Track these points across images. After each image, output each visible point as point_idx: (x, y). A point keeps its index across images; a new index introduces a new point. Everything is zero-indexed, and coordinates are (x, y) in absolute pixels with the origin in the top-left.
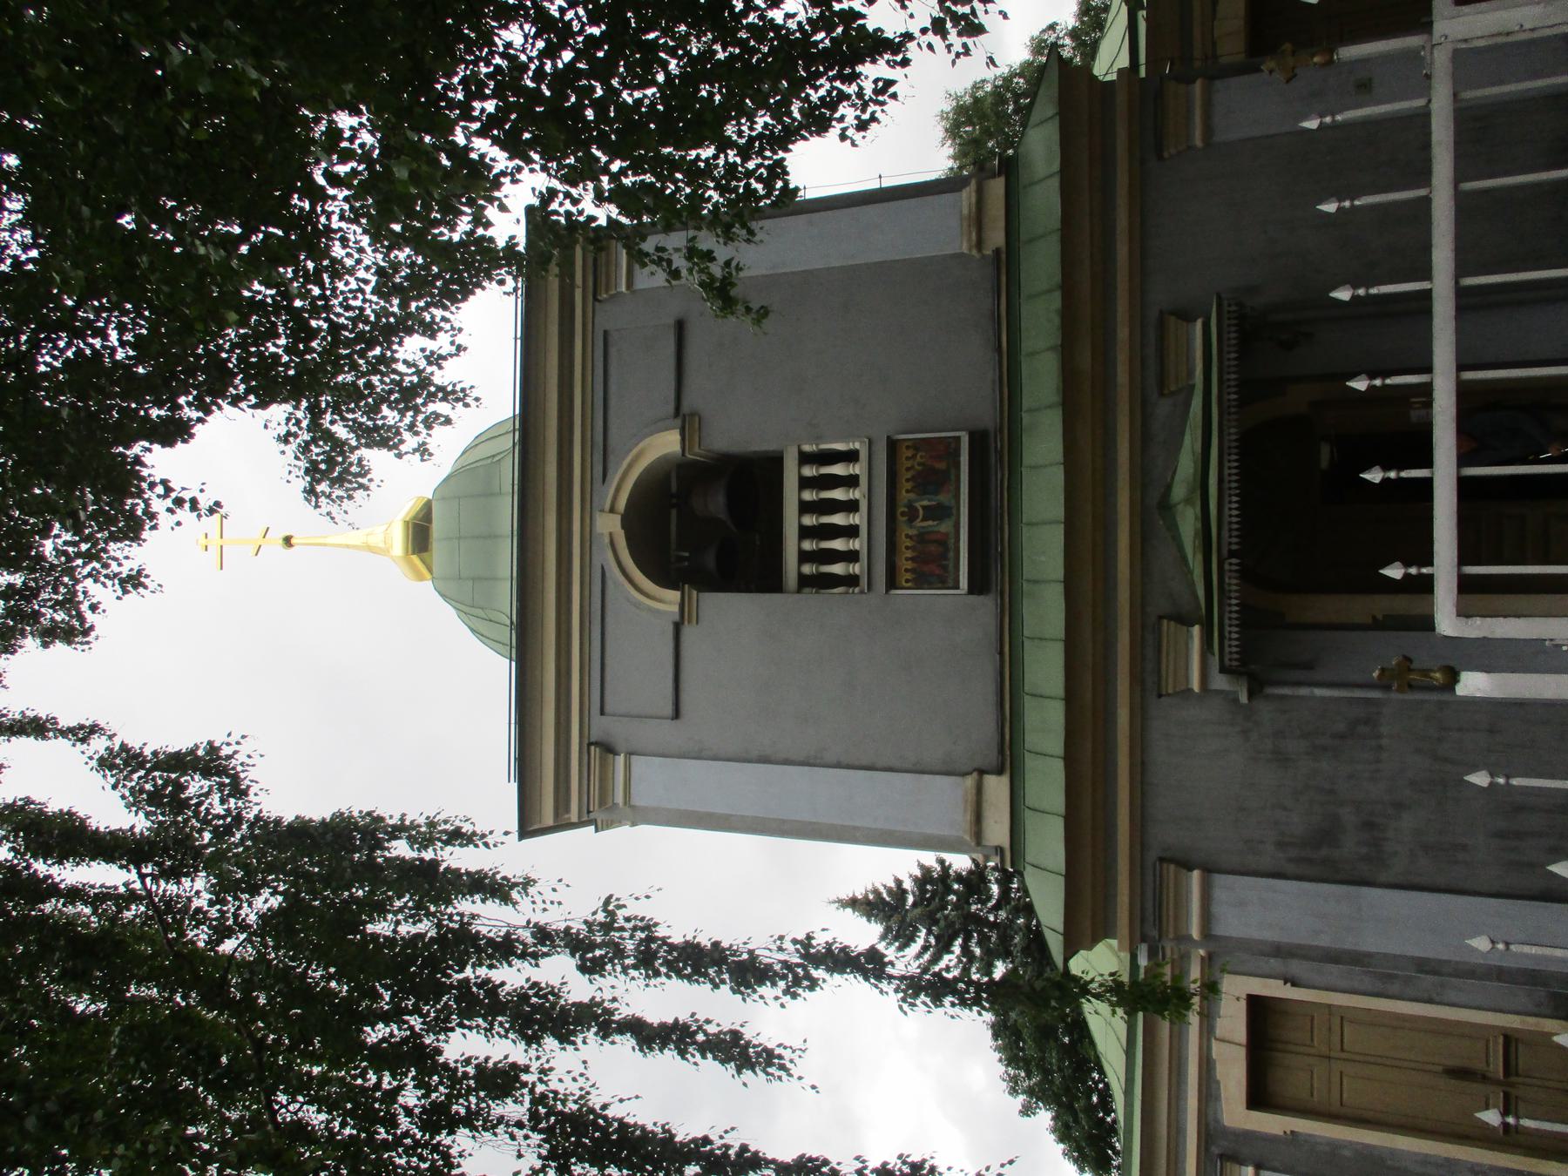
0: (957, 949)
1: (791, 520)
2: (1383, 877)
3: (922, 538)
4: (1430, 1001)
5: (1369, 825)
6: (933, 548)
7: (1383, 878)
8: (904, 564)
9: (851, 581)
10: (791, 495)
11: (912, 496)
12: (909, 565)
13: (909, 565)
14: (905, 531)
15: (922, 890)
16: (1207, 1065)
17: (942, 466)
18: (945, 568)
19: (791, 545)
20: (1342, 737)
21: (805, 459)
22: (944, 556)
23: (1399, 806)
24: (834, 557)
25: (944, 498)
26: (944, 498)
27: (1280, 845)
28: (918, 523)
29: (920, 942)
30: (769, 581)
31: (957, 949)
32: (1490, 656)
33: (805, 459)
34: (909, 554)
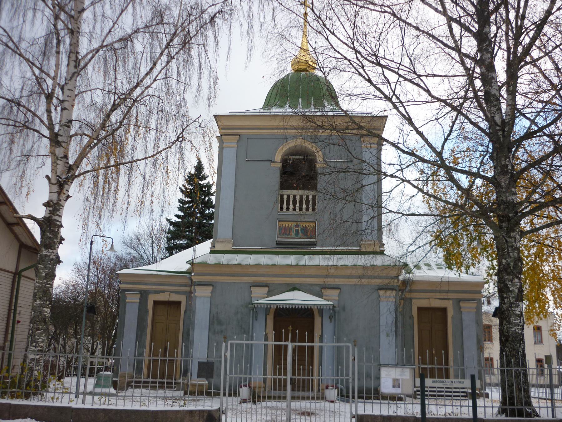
0: (187, 199)
1: (298, 193)
3: (291, 229)
5: (222, 332)
6: (288, 232)
7: (210, 334)
8: (285, 224)
9: (282, 209)
10: (305, 193)
12: (284, 226)
13: (284, 226)
14: (293, 224)
15: (205, 187)
16: (163, 292)
17: (309, 234)
18: (283, 235)
19: (292, 193)
20: (241, 326)
22: (286, 234)
25: (300, 235)
26: (300, 235)
27: (217, 313)
28: (295, 228)
29: (188, 186)
30: (284, 185)
31: (187, 199)
32: (226, 346)
33: (314, 197)
34: (287, 226)
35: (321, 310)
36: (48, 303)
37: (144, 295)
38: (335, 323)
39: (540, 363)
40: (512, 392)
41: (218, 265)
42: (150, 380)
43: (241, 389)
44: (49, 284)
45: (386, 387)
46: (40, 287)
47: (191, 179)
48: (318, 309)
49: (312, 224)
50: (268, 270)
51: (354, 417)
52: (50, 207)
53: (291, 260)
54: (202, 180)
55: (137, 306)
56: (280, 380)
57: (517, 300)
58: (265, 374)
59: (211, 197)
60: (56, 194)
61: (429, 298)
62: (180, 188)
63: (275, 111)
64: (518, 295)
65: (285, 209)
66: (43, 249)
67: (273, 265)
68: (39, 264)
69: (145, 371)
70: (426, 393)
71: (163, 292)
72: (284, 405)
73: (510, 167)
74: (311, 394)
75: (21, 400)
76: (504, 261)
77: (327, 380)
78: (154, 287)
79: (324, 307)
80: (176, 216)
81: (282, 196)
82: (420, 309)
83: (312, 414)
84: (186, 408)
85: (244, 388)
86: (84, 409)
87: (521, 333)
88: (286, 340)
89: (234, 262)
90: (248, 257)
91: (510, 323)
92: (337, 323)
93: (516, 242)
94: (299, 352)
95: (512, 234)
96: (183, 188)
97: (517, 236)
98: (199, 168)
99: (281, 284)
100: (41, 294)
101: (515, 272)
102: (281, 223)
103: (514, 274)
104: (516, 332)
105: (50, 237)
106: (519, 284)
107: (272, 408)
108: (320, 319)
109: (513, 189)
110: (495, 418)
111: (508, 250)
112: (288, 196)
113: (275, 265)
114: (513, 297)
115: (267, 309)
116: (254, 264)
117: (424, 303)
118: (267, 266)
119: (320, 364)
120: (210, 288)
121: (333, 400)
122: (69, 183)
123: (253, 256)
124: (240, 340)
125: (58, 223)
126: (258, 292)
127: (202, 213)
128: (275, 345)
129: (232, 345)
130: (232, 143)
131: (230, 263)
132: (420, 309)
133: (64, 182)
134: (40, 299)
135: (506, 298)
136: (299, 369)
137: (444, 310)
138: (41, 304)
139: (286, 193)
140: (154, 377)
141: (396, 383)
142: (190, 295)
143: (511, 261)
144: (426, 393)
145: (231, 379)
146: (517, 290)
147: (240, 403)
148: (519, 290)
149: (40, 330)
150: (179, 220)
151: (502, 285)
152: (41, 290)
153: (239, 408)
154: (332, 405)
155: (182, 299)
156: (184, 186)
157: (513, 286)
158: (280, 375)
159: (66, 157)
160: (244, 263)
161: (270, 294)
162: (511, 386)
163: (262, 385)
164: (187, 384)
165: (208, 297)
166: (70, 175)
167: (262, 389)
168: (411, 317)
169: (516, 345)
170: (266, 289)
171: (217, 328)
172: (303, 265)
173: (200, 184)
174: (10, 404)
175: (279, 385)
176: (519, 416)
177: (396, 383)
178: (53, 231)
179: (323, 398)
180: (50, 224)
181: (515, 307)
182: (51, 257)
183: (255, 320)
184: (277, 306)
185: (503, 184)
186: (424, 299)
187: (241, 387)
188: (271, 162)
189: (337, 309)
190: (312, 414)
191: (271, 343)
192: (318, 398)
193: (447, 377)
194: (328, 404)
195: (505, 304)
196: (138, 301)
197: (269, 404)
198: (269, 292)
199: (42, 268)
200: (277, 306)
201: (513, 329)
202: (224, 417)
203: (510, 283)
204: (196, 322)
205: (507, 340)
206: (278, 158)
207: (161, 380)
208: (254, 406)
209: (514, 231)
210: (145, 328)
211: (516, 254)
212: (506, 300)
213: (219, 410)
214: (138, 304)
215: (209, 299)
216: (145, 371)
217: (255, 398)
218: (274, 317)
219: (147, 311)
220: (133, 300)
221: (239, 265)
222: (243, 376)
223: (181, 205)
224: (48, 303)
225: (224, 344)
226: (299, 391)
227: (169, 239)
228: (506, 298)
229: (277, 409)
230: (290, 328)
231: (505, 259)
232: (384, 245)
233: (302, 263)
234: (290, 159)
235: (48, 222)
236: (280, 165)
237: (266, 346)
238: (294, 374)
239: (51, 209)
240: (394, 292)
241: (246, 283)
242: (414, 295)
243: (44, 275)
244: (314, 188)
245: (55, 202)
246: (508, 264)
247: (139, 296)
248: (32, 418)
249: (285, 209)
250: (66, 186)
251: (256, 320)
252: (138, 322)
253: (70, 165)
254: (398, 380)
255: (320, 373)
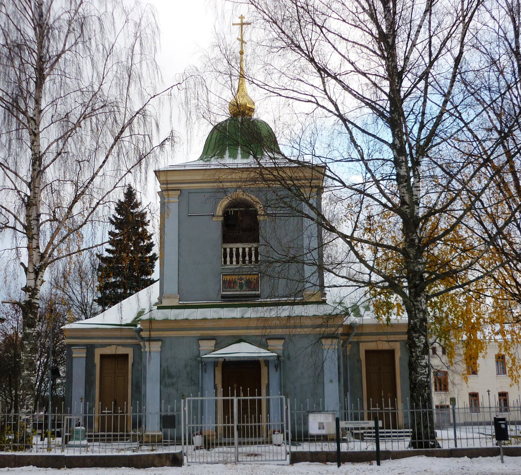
1: (240, 246)
2: (162, 387)
3: (235, 282)
4: (132, 396)
5: (173, 384)
7: (162, 387)
8: (228, 278)
9: (225, 262)
10: (247, 246)
11: (245, 280)
12: (228, 279)
15: (137, 216)
16: (110, 345)
19: (234, 246)
20: (191, 379)
21: (256, 249)
22: (230, 288)
23: (177, 390)
24: (231, 257)
25: (245, 288)
26: (245, 288)
27: (167, 367)
29: (119, 217)
30: (226, 238)
31: (117, 231)
33: (256, 249)
35: (267, 362)
36: (33, 372)
37: (90, 349)
38: (280, 370)
39: (504, 397)
40: (419, 429)
41: (166, 321)
42: (100, 433)
43: (194, 438)
44: (34, 357)
45: (314, 429)
46: (27, 360)
47: (121, 208)
48: (265, 361)
49: (255, 277)
50: (214, 324)
51: (288, 454)
52: (29, 292)
53: (236, 313)
54: (133, 209)
55: (83, 361)
56: (229, 427)
57: (423, 354)
58: (216, 423)
59: (145, 227)
60: (34, 281)
61: (376, 341)
62: (109, 218)
63: (214, 163)
64: (423, 349)
65: (228, 263)
66: (27, 328)
67: (219, 319)
68: (24, 340)
69: (96, 425)
70: (374, 434)
71: (110, 345)
72: (233, 450)
73: (417, 241)
74: (261, 440)
75: (23, 452)
76: (412, 321)
77: (274, 425)
78: (100, 341)
79: (270, 359)
80: (107, 250)
81: (225, 249)
82: (367, 352)
83: (259, 455)
84: (154, 452)
85: (198, 436)
86: (74, 456)
87: (427, 381)
88: (232, 395)
89: (181, 317)
90: (195, 312)
91: (417, 373)
92: (282, 373)
93: (421, 305)
94: (243, 405)
95: (419, 299)
96: (113, 219)
97: (423, 300)
98: (130, 194)
99: (227, 337)
100: (28, 366)
101: (421, 330)
102: (225, 277)
103: (420, 332)
104: (422, 380)
105: (32, 318)
106: (424, 340)
107: (223, 452)
108: (266, 368)
109: (419, 260)
110: (406, 450)
111: (415, 311)
112: (231, 249)
113: (221, 319)
114: (419, 352)
115: (215, 363)
116: (201, 318)
117: (372, 346)
118: (213, 320)
119: (268, 412)
120: (160, 343)
121: (279, 443)
122: (43, 270)
123: (200, 310)
124: (195, 397)
125: (37, 305)
126: (206, 345)
127: (136, 244)
128: (224, 400)
129: (189, 401)
130: (174, 198)
131: (178, 318)
132: (367, 352)
133: (39, 269)
134: (27, 369)
135: (414, 352)
136: (251, 417)
137: (391, 353)
138: (28, 374)
139: (228, 246)
140: (115, 430)
141: (321, 426)
142: (137, 348)
143: (418, 321)
144: (374, 434)
145: (189, 428)
146: (422, 346)
147: (194, 450)
148: (424, 345)
149: (28, 395)
150: (111, 255)
151: (411, 342)
152: (28, 362)
153: (194, 453)
154: (279, 448)
155: (129, 351)
156: (114, 216)
157: (420, 342)
158: (229, 423)
159: (38, 247)
160: (191, 318)
161: (218, 347)
162: (419, 424)
163: (215, 433)
164: (142, 435)
165: (157, 352)
166: (43, 263)
167: (215, 437)
168: (359, 361)
169: (422, 391)
170: (213, 343)
171: (168, 381)
172: (248, 318)
173: (132, 213)
174: (15, 456)
175: (228, 432)
176: (425, 448)
177: (321, 426)
178: (34, 312)
179: (271, 443)
180: (31, 307)
181: (421, 360)
182: (34, 334)
183: (204, 371)
184: (225, 359)
185: (411, 255)
186: (372, 341)
187: (194, 436)
188: (213, 216)
189: (282, 358)
190: (259, 455)
191: (220, 398)
192: (267, 443)
193: (362, 419)
194: (275, 447)
195: (413, 357)
196: (85, 355)
197: (221, 449)
198: (216, 344)
199: (26, 344)
200: (225, 359)
201: (420, 378)
202: (185, 457)
203: (417, 340)
204: (148, 376)
205: (415, 387)
206: (219, 211)
207: (121, 433)
208: (208, 452)
209: (420, 296)
210: (94, 382)
211: (421, 316)
212: (414, 354)
213: (181, 452)
214: (85, 359)
215: (159, 354)
216: (96, 425)
217: (208, 445)
218: (222, 369)
219: (94, 366)
220: (80, 354)
221: (187, 320)
222: (195, 425)
223: (112, 238)
224: (33, 372)
225: (182, 401)
226: (248, 437)
227: (100, 278)
228: (414, 352)
229: (228, 453)
230: (235, 385)
231: (413, 320)
232: (326, 294)
233: (247, 315)
234: (231, 212)
235: (29, 305)
236: (221, 219)
237: (216, 401)
238: (239, 422)
239: (30, 293)
240: (335, 341)
241: (194, 337)
242: (363, 338)
243: (29, 349)
244: (256, 240)
245: (33, 287)
246: (415, 324)
247: (85, 351)
248: (34, 466)
249: (228, 263)
250: (41, 273)
251: (205, 372)
252: (86, 377)
253: (42, 254)
254: (322, 423)
255: (268, 419)
